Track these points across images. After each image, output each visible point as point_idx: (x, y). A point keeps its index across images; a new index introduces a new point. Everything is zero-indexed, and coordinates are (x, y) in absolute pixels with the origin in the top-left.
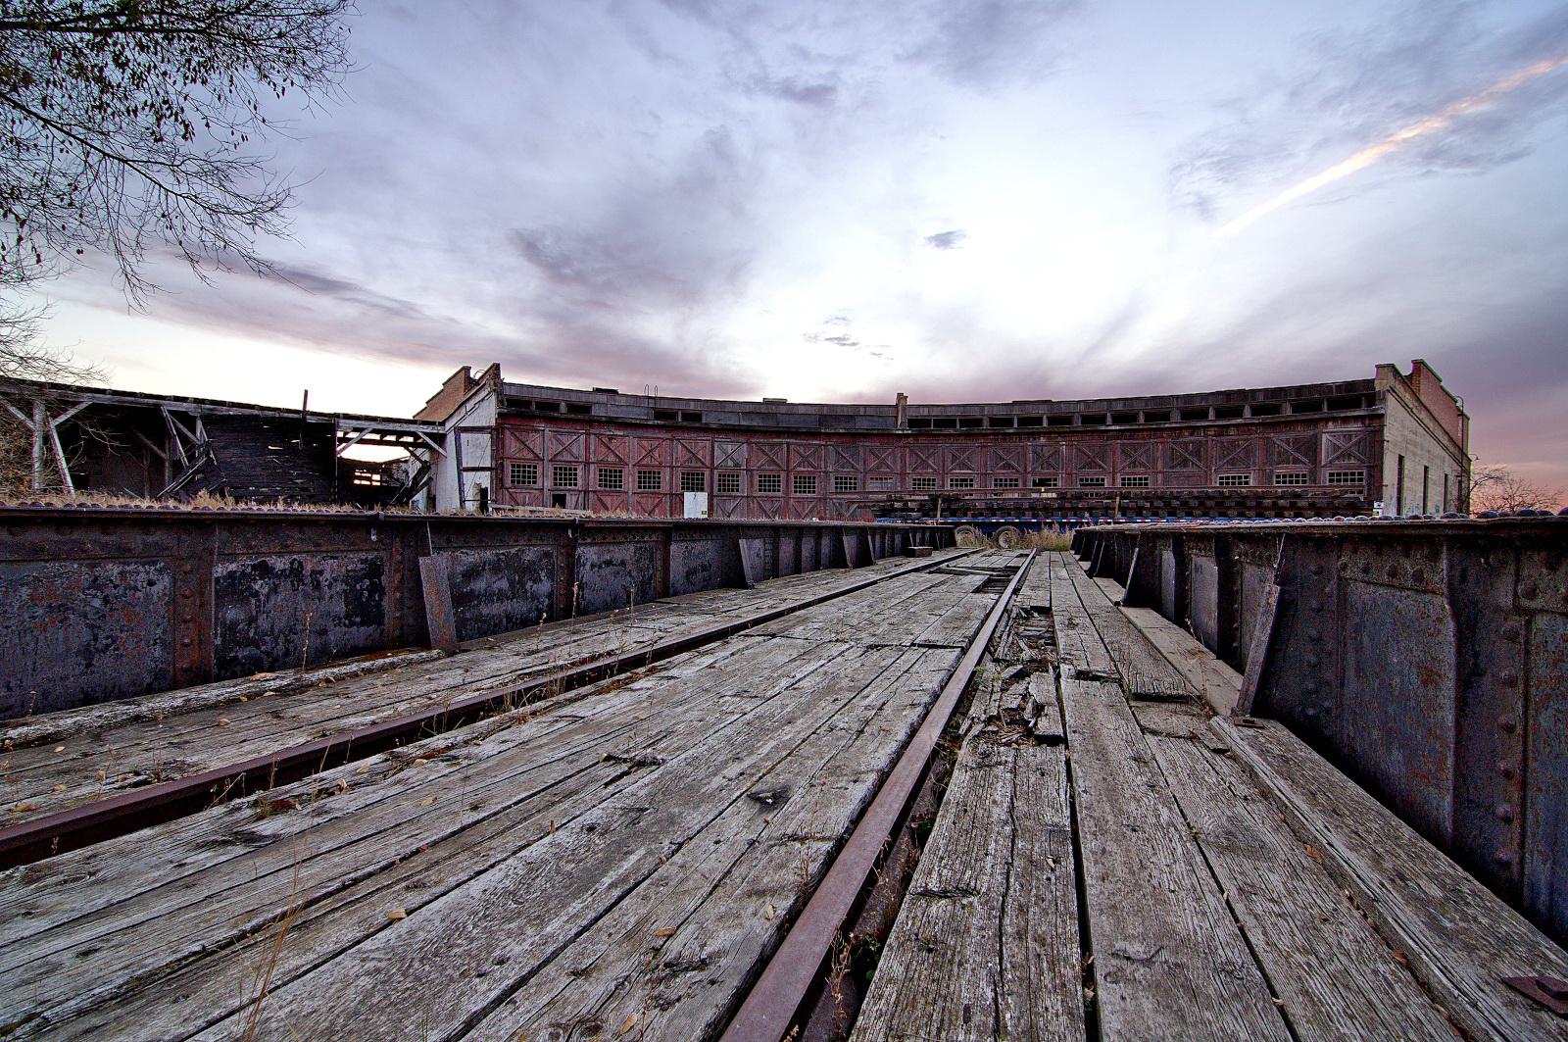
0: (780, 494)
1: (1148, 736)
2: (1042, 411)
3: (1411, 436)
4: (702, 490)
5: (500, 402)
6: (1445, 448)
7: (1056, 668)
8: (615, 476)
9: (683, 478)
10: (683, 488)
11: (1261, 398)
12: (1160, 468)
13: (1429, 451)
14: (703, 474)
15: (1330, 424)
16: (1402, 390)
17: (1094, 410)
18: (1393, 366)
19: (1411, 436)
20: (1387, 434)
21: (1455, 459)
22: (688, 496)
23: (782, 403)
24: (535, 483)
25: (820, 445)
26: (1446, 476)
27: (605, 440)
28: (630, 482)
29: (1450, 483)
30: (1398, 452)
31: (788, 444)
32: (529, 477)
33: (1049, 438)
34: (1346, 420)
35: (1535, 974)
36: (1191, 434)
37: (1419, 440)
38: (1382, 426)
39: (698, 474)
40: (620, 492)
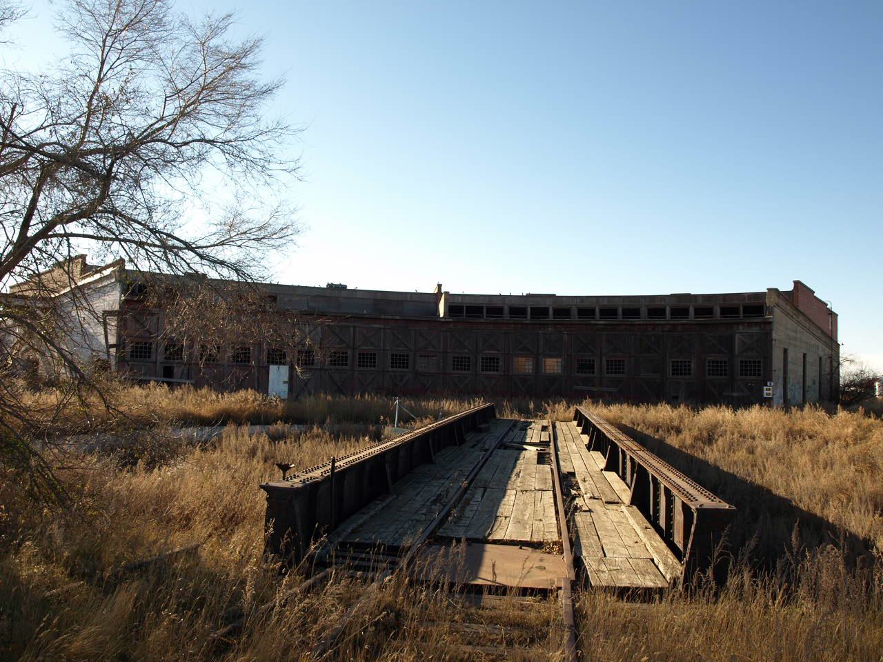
0: (347, 368)
1: (84, 74)
2: (548, 303)
3: (793, 334)
5: (124, 291)
6: (819, 339)
7: (583, 496)
10: (268, 362)
11: (700, 301)
13: (806, 343)
15: (741, 327)
16: (784, 304)
17: (586, 305)
19: (793, 334)
20: (774, 336)
21: (826, 345)
23: (343, 287)
24: (149, 357)
25: (381, 328)
26: (820, 358)
29: (823, 362)
30: (783, 346)
32: (145, 352)
34: (750, 325)
35: (24, 155)
37: (798, 336)
38: (771, 330)
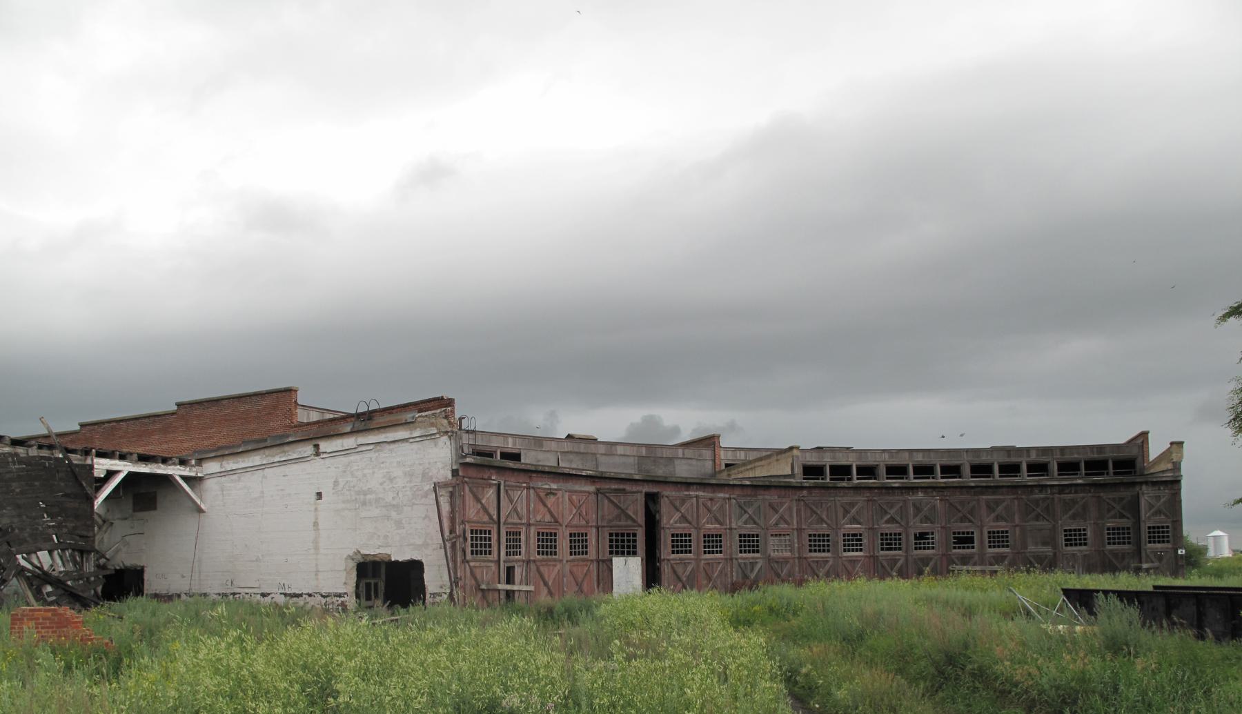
4: (635, 554)
8: (629, 541)
9: (611, 541)
10: (611, 553)
12: (1017, 521)
14: (635, 535)
18: (1172, 444)
22: (618, 562)
27: (542, 495)
28: (563, 544)
31: (697, 497)
33: (926, 493)
36: (1041, 492)
39: (628, 535)
40: (555, 560)
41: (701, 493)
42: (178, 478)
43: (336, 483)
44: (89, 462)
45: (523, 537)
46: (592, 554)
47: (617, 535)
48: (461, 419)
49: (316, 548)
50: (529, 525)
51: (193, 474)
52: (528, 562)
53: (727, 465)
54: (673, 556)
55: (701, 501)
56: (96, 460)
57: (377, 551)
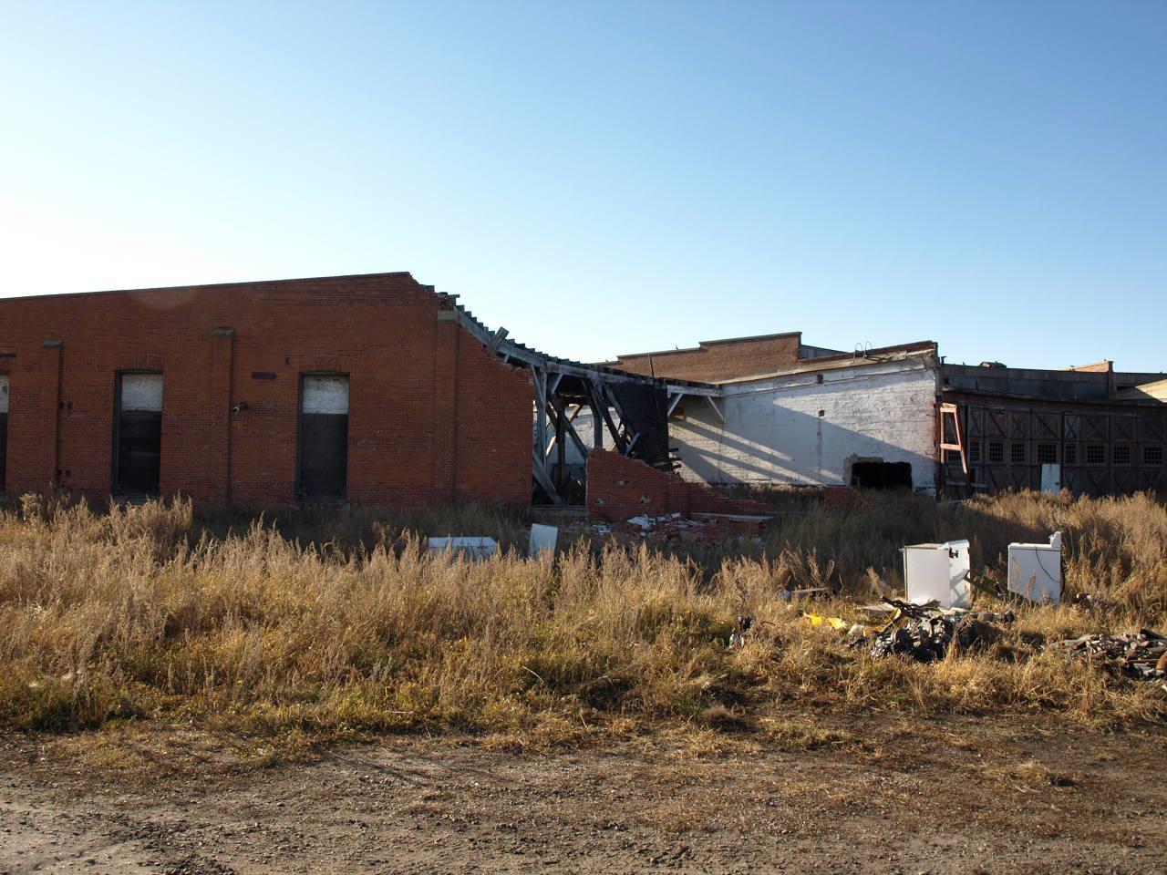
4: (1054, 462)
22: (1045, 467)
39: (1051, 447)
41: (1112, 414)
42: (710, 399)
43: (836, 404)
44: (664, 387)
45: (980, 446)
46: (1027, 462)
47: (1043, 446)
48: (943, 358)
49: (820, 453)
50: (985, 437)
51: (717, 396)
52: (984, 465)
53: (1119, 388)
54: (1088, 464)
55: (1112, 419)
56: (668, 386)
57: (872, 455)
